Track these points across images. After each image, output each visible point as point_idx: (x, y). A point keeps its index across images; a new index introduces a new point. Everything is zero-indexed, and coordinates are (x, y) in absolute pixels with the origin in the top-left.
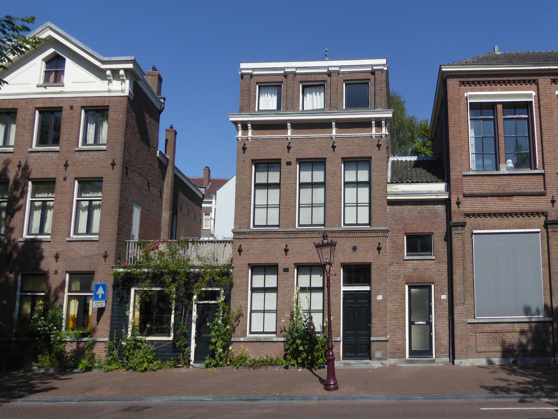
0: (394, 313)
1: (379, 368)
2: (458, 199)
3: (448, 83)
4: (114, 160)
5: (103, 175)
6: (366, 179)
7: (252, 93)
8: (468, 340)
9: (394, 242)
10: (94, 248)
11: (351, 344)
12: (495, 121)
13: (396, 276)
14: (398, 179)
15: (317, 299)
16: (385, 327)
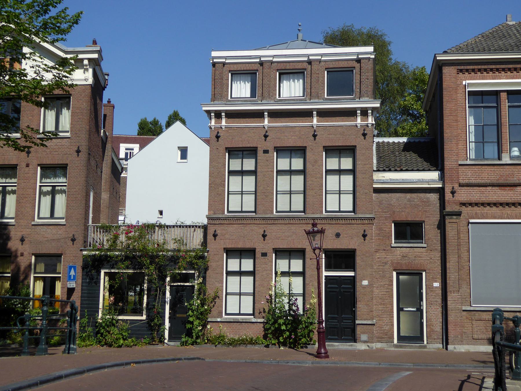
0: (380, 298)
1: (365, 350)
2: (453, 188)
3: (444, 71)
4: (78, 147)
5: (67, 162)
6: (350, 167)
7: (225, 82)
8: (463, 327)
9: (380, 229)
10: (61, 231)
11: (332, 328)
12: (498, 108)
13: (383, 263)
14: (385, 166)
15: (297, 283)
16: (372, 311)
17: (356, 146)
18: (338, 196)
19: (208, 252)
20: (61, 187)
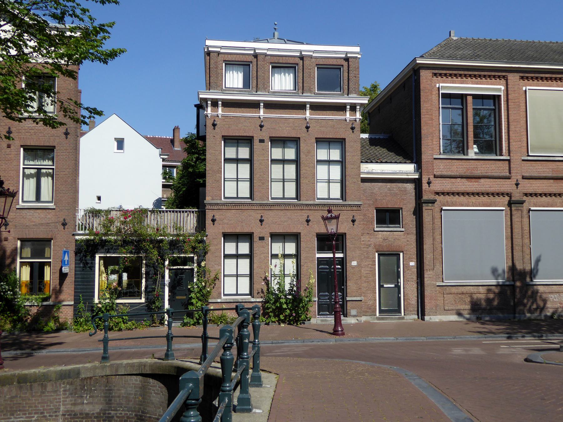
2: (429, 179)
3: (421, 74)
5: (55, 144)
6: (247, 156)
7: (219, 71)
10: (50, 216)
13: (367, 245)
15: (290, 266)
17: (253, 137)
18: (327, 183)
19: (207, 236)
20: (47, 170)
